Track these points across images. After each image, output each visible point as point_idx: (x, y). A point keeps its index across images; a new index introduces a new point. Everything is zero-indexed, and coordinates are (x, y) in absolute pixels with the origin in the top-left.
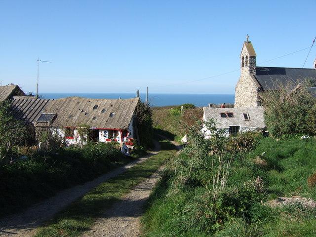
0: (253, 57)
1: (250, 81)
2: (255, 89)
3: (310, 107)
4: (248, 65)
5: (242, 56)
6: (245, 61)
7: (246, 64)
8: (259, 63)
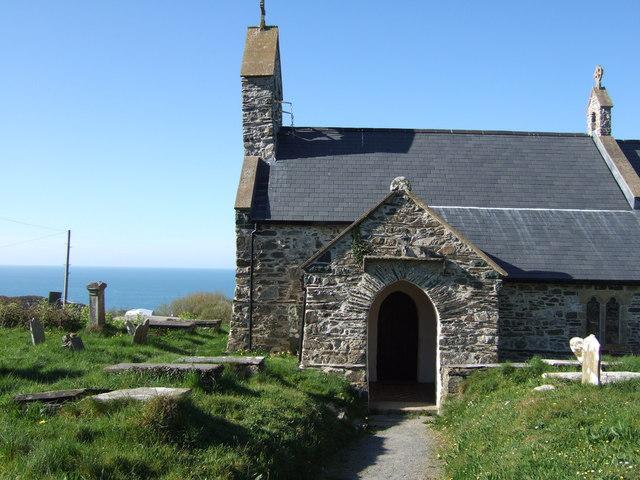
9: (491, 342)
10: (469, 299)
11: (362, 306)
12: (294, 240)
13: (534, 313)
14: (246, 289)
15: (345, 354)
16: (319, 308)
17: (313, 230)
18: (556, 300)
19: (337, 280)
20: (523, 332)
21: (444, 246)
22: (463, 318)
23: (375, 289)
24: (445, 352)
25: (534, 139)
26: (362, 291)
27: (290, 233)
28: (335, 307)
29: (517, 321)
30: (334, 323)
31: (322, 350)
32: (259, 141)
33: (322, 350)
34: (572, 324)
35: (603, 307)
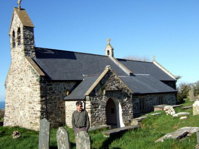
0: (29, 29)
1: (26, 68)
2: (35, 79)
3: (152, 99)
4: (22, 41)
5: (12, 30)
6: (16, 37)
7: (19, 41)
8: (39, 43)
9: (132, 112)
10: (126, 101)
11: (104, 106)
12: (58, 87)
14: (44, 106)
15: (102, 122)
16: (94, 108)
17: (63, 83)
19: (97, 98)
21: (120, 86)
22: (126, 106)
24: (190, 106)
25: (97, 56)
26: (104, 101)
27: (57, 85)
28: (98, 107)
30: (98, 112)
31: (96, 122)
32: (30, 51)
33: (96, 122)
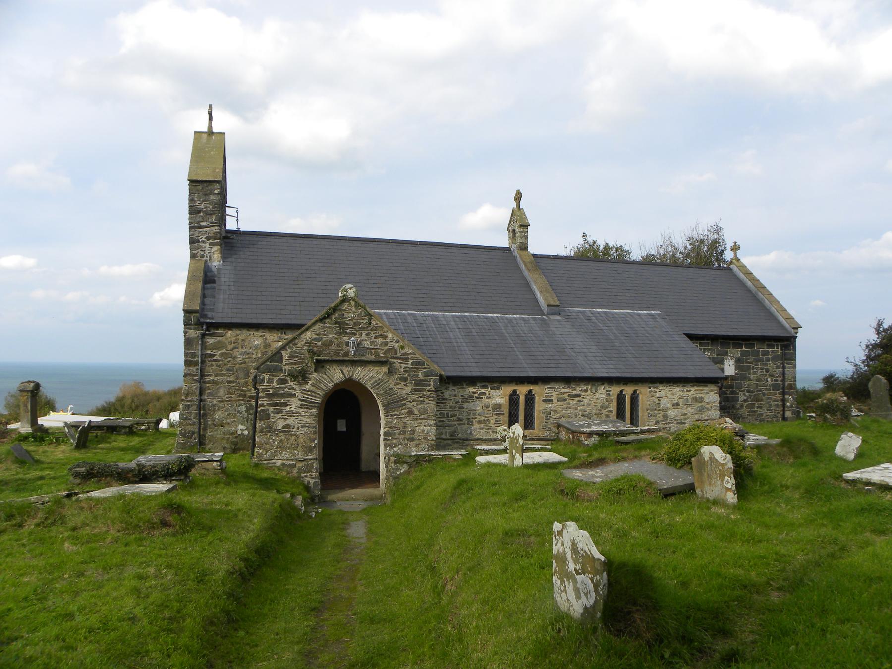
11: (314, 403)
13: (465, 405)
18: (484, 394)
20: (456, 423)
23: (325, 388)
25: (323, 242)
29: (451, 413)
34: (496, 414)
35: (522, 399)
